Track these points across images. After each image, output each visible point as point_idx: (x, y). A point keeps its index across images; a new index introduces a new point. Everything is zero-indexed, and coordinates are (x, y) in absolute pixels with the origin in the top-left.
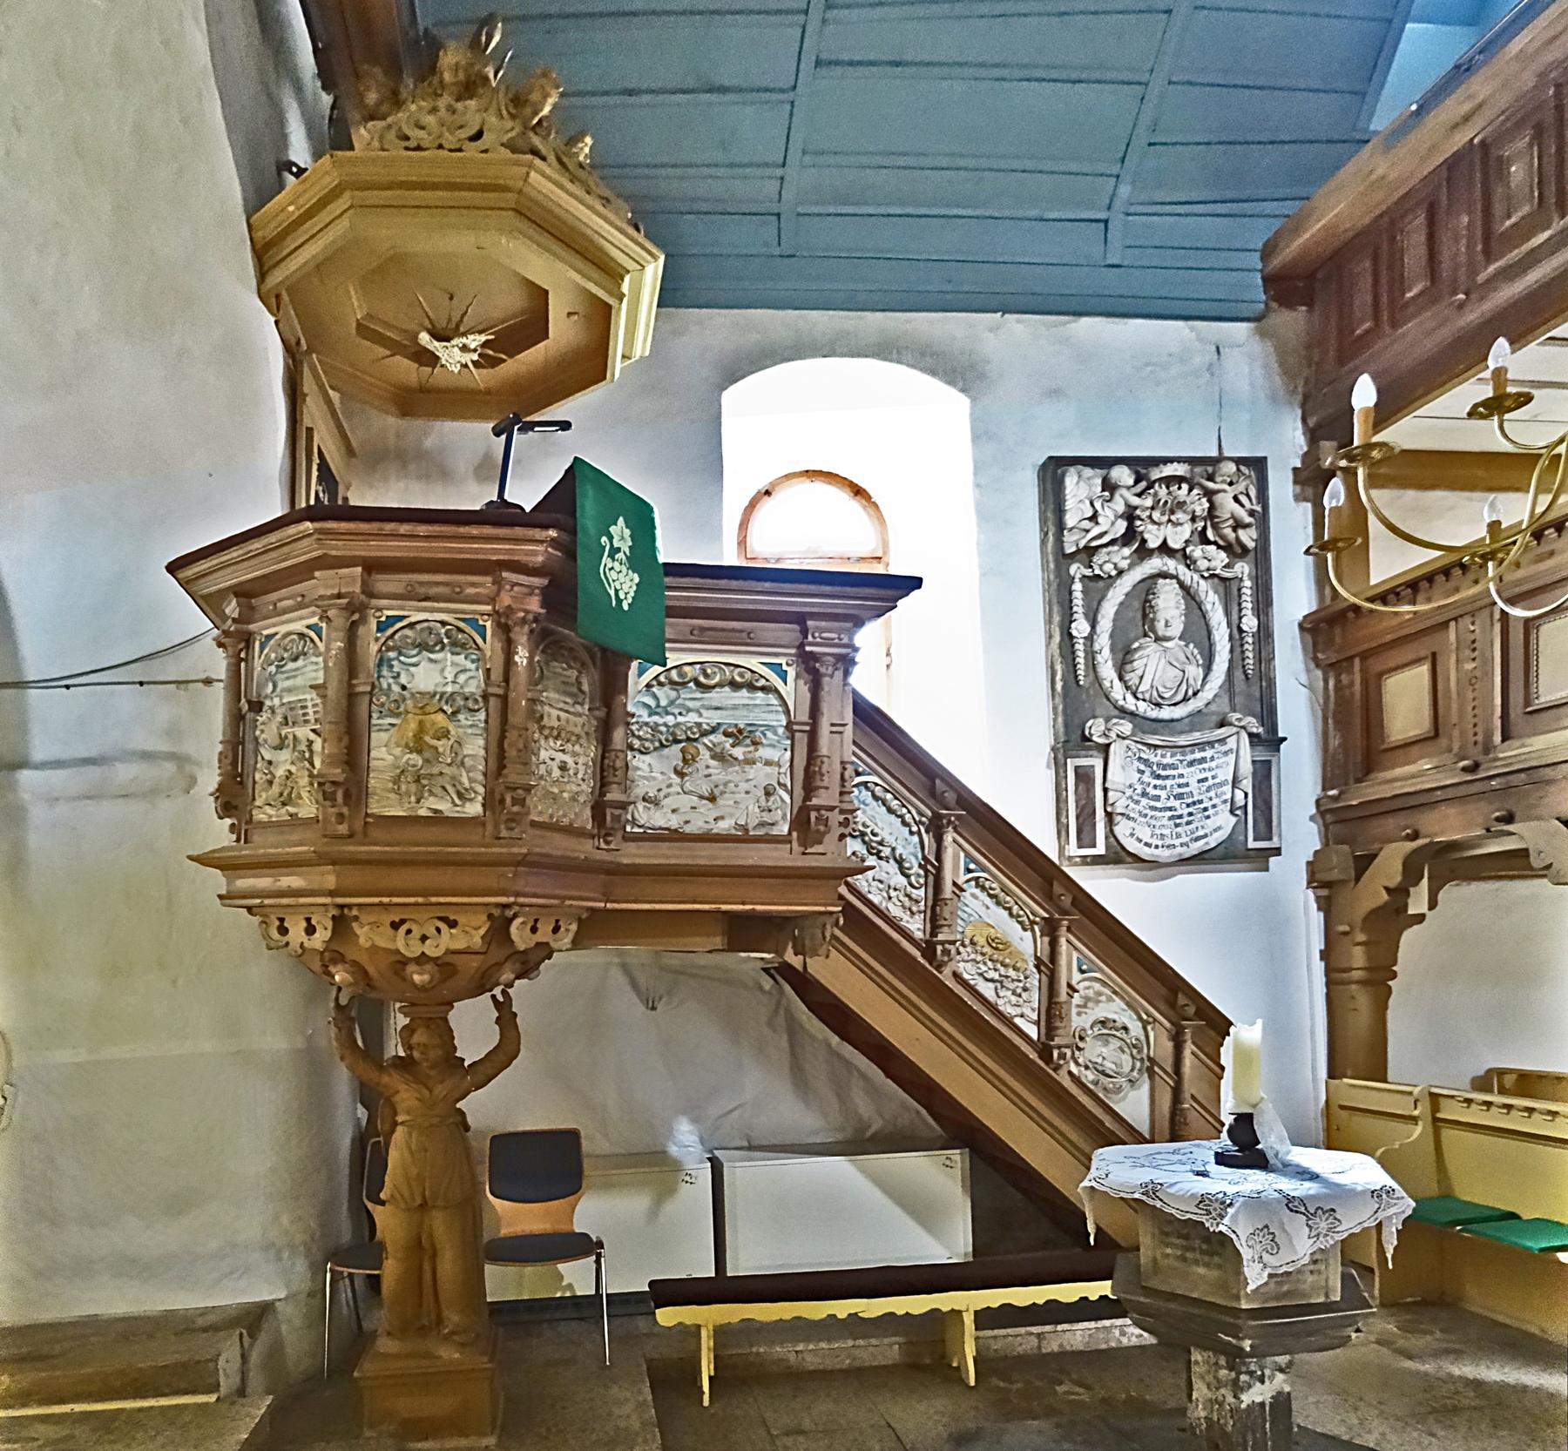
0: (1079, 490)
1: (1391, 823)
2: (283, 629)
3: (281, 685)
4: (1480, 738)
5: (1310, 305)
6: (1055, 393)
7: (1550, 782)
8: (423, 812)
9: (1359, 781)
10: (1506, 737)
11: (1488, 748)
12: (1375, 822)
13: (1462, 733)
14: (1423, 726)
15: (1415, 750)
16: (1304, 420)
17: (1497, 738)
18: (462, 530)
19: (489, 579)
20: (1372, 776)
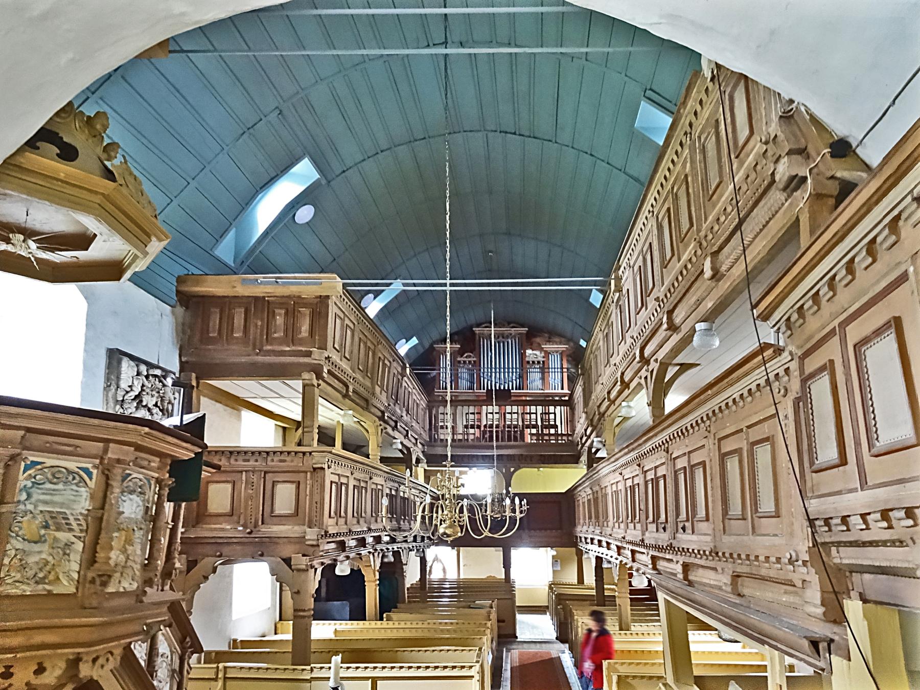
0: (127, 369)
1: (208, 549)
2: (50, 462)
3: (35, 497)
4: (253, 521)
5: (187, 308)
6: (115, 313)
7: (277, 543)
8: (122, 590)
9: (193, 527)
10: (263, 523)
11: (256, 526)
12: (200, 546)
13: (245, 516)
14: (227, 508)
15: (221, 519)
16: (180, 356)
17: (260, 523)
18: (185, 445)
19: (158, 459)
20: (200, 525)
